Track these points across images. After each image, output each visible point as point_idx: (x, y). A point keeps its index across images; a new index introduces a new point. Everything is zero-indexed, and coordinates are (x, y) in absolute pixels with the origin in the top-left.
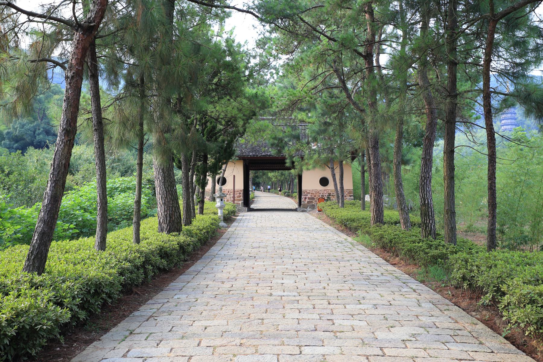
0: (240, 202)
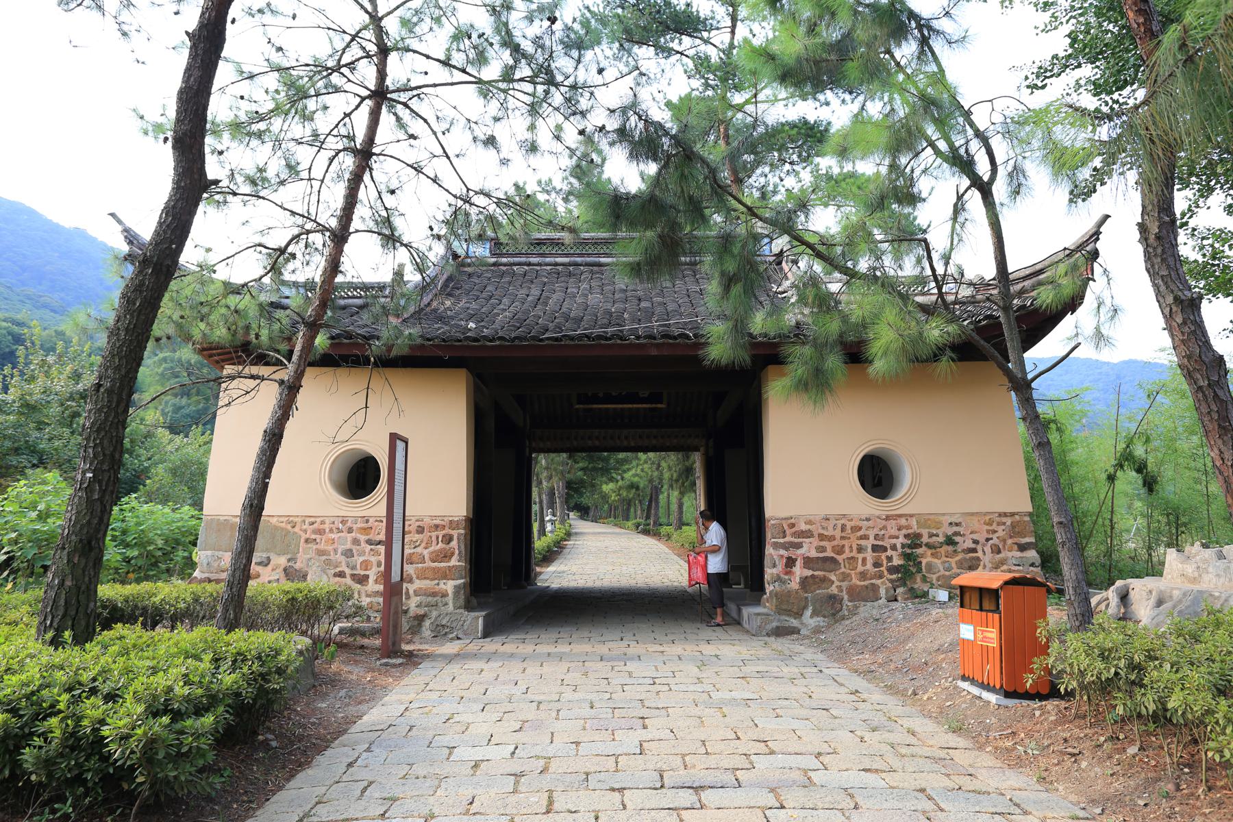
0: (449, 586)
